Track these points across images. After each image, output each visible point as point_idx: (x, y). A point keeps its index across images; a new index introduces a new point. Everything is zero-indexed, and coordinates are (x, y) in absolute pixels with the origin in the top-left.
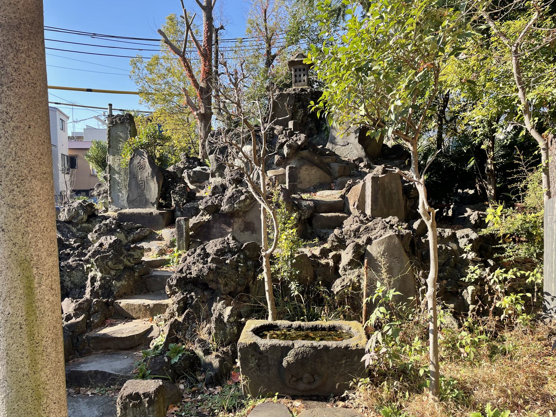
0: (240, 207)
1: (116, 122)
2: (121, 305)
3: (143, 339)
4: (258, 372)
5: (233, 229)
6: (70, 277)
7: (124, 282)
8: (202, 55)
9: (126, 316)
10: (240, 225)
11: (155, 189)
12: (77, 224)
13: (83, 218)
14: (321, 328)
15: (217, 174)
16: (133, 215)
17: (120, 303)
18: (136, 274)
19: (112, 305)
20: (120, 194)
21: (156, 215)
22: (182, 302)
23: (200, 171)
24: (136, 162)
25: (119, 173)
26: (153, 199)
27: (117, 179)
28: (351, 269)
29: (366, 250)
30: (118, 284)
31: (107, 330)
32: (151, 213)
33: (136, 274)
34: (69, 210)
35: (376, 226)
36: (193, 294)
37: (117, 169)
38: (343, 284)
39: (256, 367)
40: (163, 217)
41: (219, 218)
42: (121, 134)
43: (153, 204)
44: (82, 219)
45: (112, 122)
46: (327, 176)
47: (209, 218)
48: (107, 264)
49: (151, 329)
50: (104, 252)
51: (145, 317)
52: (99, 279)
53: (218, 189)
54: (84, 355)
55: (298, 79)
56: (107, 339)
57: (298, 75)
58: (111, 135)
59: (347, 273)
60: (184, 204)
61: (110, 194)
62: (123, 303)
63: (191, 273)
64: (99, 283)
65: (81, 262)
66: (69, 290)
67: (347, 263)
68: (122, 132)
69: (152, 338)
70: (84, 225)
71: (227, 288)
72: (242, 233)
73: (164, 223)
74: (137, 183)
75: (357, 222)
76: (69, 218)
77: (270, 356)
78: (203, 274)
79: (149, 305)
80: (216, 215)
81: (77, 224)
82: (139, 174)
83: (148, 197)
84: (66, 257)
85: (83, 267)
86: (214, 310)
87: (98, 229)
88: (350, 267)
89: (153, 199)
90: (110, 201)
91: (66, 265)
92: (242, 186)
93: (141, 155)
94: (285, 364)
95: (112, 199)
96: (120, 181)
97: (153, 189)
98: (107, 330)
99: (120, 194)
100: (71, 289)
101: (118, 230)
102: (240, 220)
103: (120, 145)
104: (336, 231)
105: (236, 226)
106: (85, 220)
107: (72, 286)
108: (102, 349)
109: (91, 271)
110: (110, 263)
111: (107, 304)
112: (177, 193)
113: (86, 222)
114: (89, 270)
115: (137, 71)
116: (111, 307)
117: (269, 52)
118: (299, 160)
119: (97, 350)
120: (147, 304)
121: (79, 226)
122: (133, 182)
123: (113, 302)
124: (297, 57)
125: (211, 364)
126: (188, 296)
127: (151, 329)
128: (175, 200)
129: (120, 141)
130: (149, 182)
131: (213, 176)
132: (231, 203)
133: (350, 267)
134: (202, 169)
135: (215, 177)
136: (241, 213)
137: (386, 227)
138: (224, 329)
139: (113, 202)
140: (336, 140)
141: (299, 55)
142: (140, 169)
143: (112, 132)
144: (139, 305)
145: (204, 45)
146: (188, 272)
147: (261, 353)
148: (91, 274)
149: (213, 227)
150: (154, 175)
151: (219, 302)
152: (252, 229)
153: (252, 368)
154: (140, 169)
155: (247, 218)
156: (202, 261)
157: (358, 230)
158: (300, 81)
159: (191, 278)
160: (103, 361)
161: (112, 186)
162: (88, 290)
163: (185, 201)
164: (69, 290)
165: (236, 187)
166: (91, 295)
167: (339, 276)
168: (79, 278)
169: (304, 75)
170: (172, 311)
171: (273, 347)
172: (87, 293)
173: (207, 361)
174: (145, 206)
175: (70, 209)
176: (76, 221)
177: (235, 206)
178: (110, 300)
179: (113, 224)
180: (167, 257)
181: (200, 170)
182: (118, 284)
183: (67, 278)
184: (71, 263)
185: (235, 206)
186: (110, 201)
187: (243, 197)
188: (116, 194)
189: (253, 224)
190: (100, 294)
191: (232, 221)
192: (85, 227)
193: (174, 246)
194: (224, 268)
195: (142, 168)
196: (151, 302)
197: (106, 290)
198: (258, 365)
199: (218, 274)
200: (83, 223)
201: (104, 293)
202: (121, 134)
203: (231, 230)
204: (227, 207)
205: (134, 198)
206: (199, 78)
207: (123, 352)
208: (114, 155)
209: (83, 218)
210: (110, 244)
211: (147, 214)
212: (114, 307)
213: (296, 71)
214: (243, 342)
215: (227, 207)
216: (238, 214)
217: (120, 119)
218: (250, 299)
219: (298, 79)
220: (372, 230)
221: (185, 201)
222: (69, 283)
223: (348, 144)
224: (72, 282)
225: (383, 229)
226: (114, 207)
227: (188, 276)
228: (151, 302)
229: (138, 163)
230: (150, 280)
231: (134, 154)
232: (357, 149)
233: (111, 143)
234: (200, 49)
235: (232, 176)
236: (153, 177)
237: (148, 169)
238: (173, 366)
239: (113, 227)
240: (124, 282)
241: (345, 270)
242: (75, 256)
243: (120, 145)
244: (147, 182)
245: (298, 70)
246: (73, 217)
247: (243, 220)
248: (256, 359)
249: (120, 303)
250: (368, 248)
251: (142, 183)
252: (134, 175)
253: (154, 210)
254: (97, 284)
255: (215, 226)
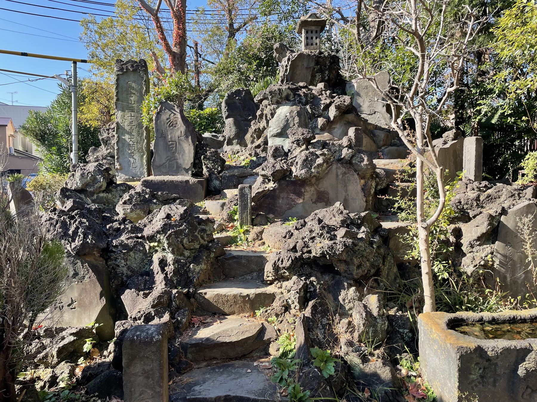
0: (318, 172)
1: (127, 69)
2: (207, 297)
3: (257, 344)
4: (481, 386)
5: (304, 199)
6: (126, 260)
7: (203, 266)
8: (176, 16)
9: (215, 312)
10: (313, 195)
11: (189, 151)
12: (92, 194)
13: (102, 186)
14: (521, 319)
15: (235, 141)
16: (163, 183)
17: (206, 294)
18: (212, 255)
19: (194, 297)
20: (132, 160)
21: (194, 184)
22: (302, 291)
23: (211, 138)
24: (164, 117)
25: (130, 133)
26: (187, 164)
27: (128, 140)
28: (480, 245)
29: (499, 222)
30: (197, 269)
31: (203, 333)
32: (187, 182)
33: (212, 255)
34: (82, 175)
35: (500, 193)
36: (313, 279)
37: (127, 128)
38: (474, 264)
39: (480, 380)
40: (202, 185)
41: (287, 186)
42: (133, 85)
43: (187, 171)
44: (100, 187)
45: (121, 69)
46: (373, 144)
47: (274, 186)
48: (182, 242)
49: (262, 330)
50: (176, 226)
51: (243, 311)
52: (171, 263)
53: (280, 152)
54: (183, 372)
55: (310, 41)
56: (209, 345)
57: (309, 38)
58: (120, 85)
59: (474, 250)
60: (219, 172)
61: (118, 158)
62: (210, 293)
63: (310, 252)
64: (172, 267)
65: (140, 240)
66: (125, 279)
67: (476, 238)
68: (134, 82)
69: (269, 342)
70: (101, 195)
71: (360, 270)
72: (314, 205)
73: (203, 193)
74: (167, 144)
75: (473, 189)
76: (83, 185)
77: (500, 363)
78: (335, 253)
79: (248, 295)
80: (283, 182)
81: (92, 194)
82: (169, 133)
83: (180, 161)
84: (114, 233)
85: (144, 247)
86: (344, 300)
87: (129, 200)
88: (478, 243)
89: (187, 164)
90: (118, 167)
91: (121, 244)
92: (314, 148)
93: (171, 108)
94: (521, 372)
95: (120, 165)
96: (131, 143)
97: (187, 152)
98: (203, 333)
99: (132, 160)
100: (128, 277)
101: (155, 201)
102: (313, 189)
103: (132, 99)
104: (111, 224)
105: (307, 196)
106: (104, 188)
107: (129, 273)
108: (205, 360)
109: (157, 251)
110: (185, 240)
111: (188, 295)
112: (209, 159)
113: (103, 191)
114: (152, 251)
115: (89, 32)
116: (192, 300)
117: (231, 25)
118: (345, 124)
119: (197, 361)
120: (245, 294)
121: (95, 197)
122: (161, 143)
123: (195, 292)
124: (310, 17)
125: (375, 375)
126: (308, 282)
127: (262, 330)
128: (207, 167)
129: (131, 93)
130: (181, 142)
131: (230, 143)
132: (307, 167)
133: (478, 243)
134: (212, 135)
135: (232, 144)
136: (313, 180)
137: (514, 195)
138: (374, 326)
139: (121, 169)
140: (362, 109)
141: (312, 15)
142: (169, 126)
143: (121, 82)
144: (235, 296)
145: (177, 6)
146: (305, 250)
147: (489, 359)
148: (156, 258)
149: (279, 198)
150: (189, 134)
151: (348, 289)
152: (326, 200)
153: (473, 381)
154: (169, 126)
155: (320, 186)
156: (329, 235)
157: (478, 199)
158: (312, 44)
159: (309, 258)
160: (221, 378)
161: (121, 149)
162: (159, 278)
163: (219, 169)
164: (125, 279)
165: (307, 149)
166: (166, 284)
167: (464, 255)
168: (138, 260)
169: (316, 38)
170: (285, 303)
171: (507, 351)
172: (158, 282)
173: (367, 370)
174: (176, 173)
175: (84, 174)
176: (92, 189)
177: (313, 170)
178: (191, 290)
179: (146, 193)
180: (230, 234)
181: (211, 136)
182: (197, 269)
183: (123, 261)
184: (126, 242)
185: (313, 170)
186: (118, 167)
187: (320, 161)
188: (126, 160)
189: (328, 194)
190: (175, 282)
191: (303, 190)
192: (103, 197)
193: (234, 220)
194: (360, 244)
195: (172, 125)
196: (252, 292)
197: (181, 277)
198: (482, 377)
199: (355, 252)
200: (100, 192)
201: (180, 281)
202: (133, 85)
203: (301, 201)
204: (303, 171)
205: (161, 163)
206: (172, 41)
207: (237, 363)
208: (123, 111)
209: (102, 186)
210: (181, 215)
211: (181, 182)
212: (196, 299)
213: (307, 32)
214: (465, 345)
215: (303, 171)
216: (310, 181)
217: (132, 66)
218: (379, 284)
219: (310, 41)
220: (495, 198)
221: (219, 169)
222: (125, 269)
223: (375, 113)
224: (128, 268)
225: (512, 196)
226: (122, 175)
227: (306, 256)
228: (252, 292)
229: (167, 119)
230: (230, 261)
231: (161, 108)
232: (385, 119)
233: (119, 94)
234: (173, 10)
235: (303, 134)
236: (187, 137)
237: (181, 127)
238: (329, 381)
239: (147, 196)
240: (203, 266)
241: (472, 246)
242: (128, 232)
243: (132, 99)
244: (179, 143)
245: (310, 32)
246: (87, 185)
247: (316, 189)
248: (480, 369)
249: (206, 294)
250: (503, 218)
251: (172, 144)
252: (162, 134)
253: (188, 177)
254: (170, 269)
255: (282, 195)
